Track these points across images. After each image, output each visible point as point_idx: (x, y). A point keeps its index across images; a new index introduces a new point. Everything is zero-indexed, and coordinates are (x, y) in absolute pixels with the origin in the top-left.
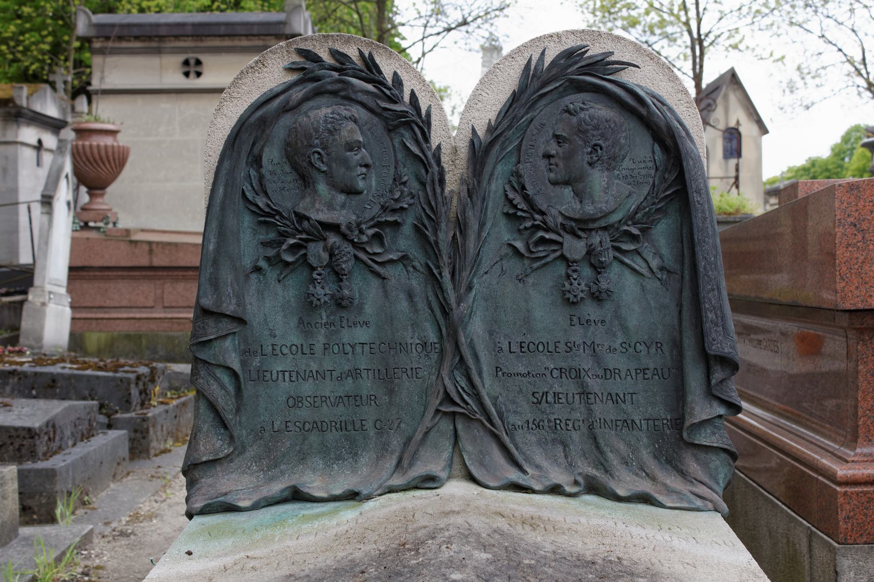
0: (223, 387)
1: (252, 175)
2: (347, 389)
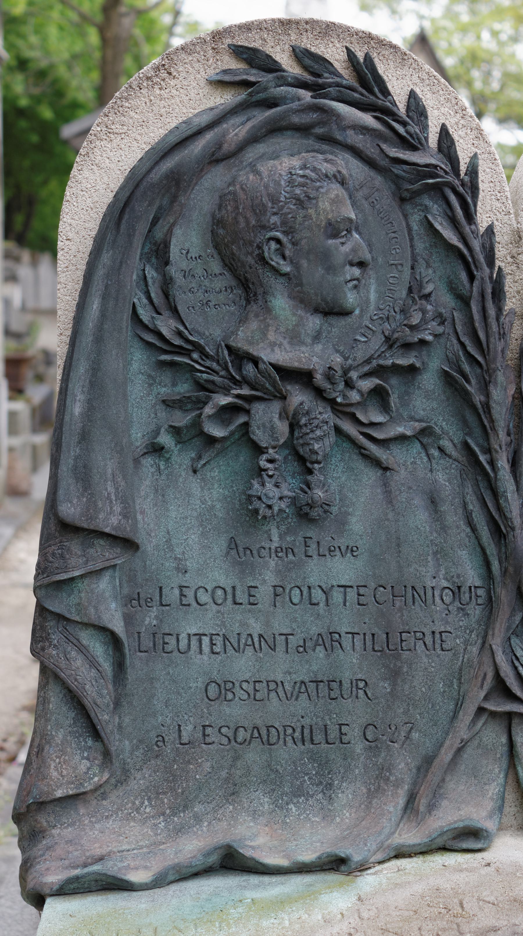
0: (93, 663)
2: (315, 668)
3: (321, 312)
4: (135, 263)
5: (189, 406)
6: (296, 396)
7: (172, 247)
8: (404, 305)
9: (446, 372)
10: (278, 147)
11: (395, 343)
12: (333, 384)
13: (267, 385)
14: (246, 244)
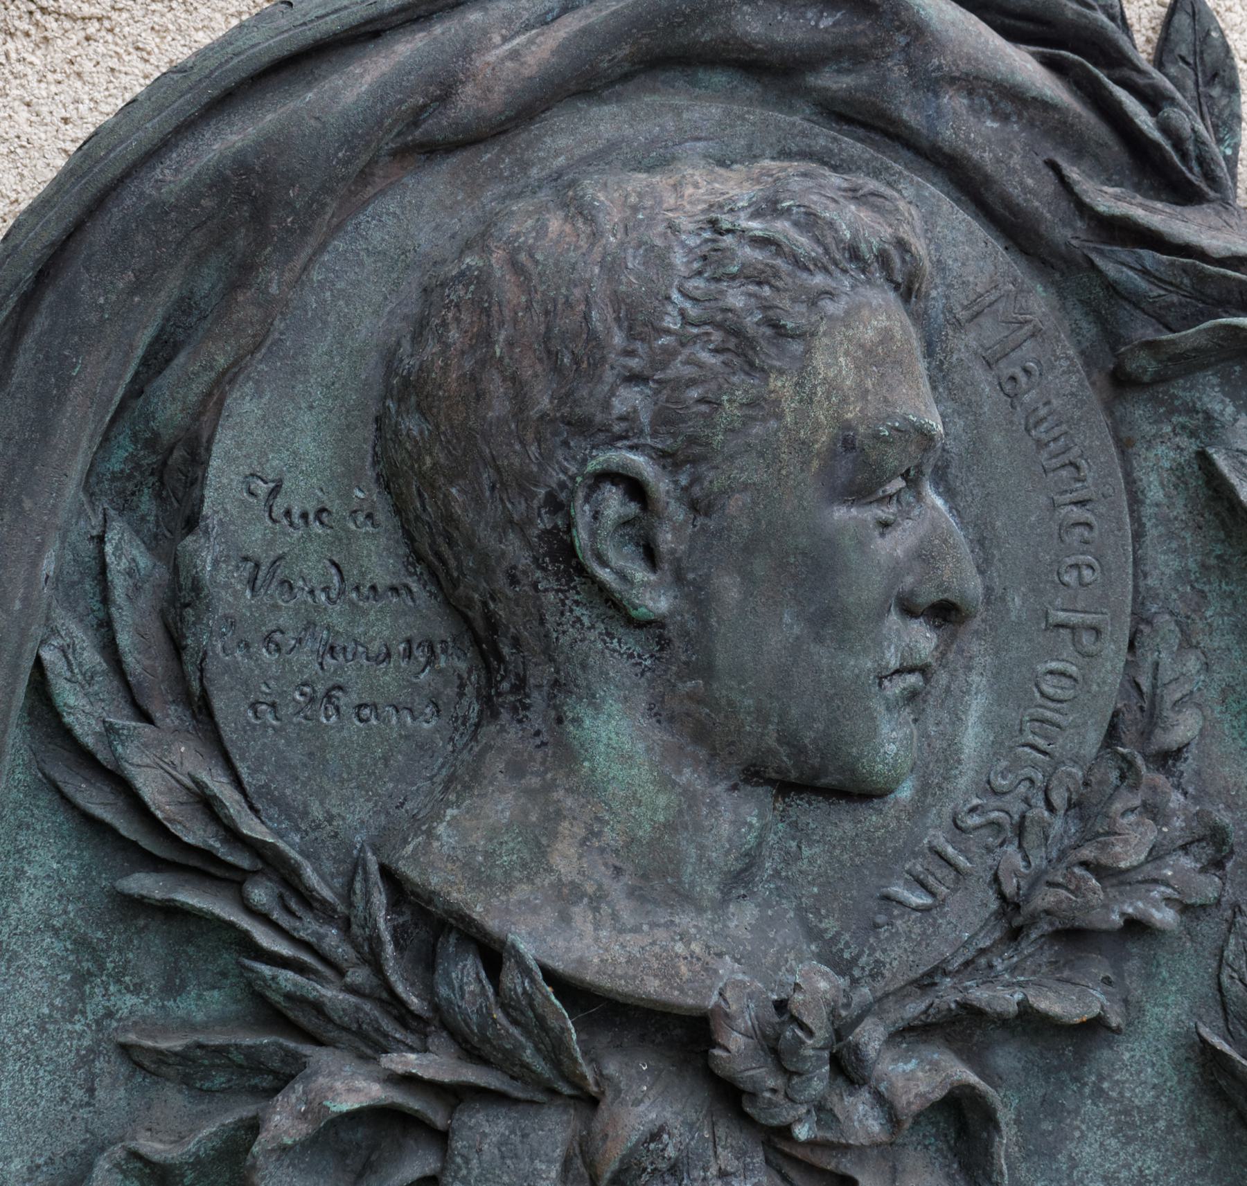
1: (117, 566)
3: (770, 782)
4: (53, 511)
5: (219, 1080)
6: (637, 1103)
7: (215, 463)
8: (1086, 784)
9: (1205, 1047)
10: (670, 126)
11: (1034, 919)
12: (789, 1074)
13: (528, 1055)
14: (505, 486)
